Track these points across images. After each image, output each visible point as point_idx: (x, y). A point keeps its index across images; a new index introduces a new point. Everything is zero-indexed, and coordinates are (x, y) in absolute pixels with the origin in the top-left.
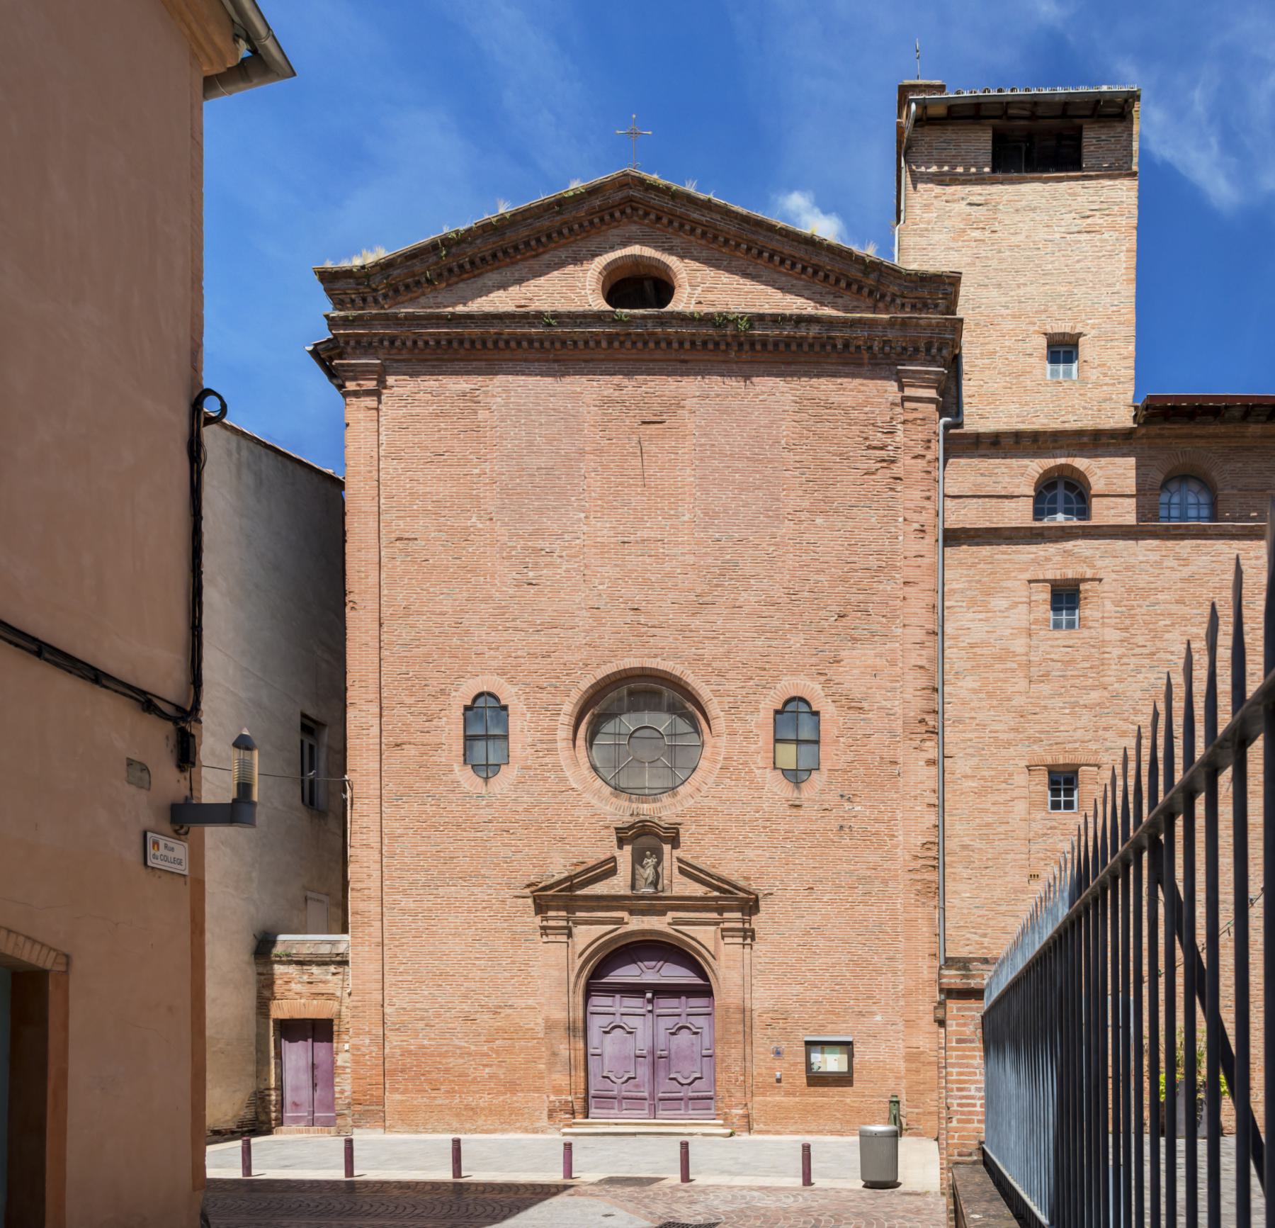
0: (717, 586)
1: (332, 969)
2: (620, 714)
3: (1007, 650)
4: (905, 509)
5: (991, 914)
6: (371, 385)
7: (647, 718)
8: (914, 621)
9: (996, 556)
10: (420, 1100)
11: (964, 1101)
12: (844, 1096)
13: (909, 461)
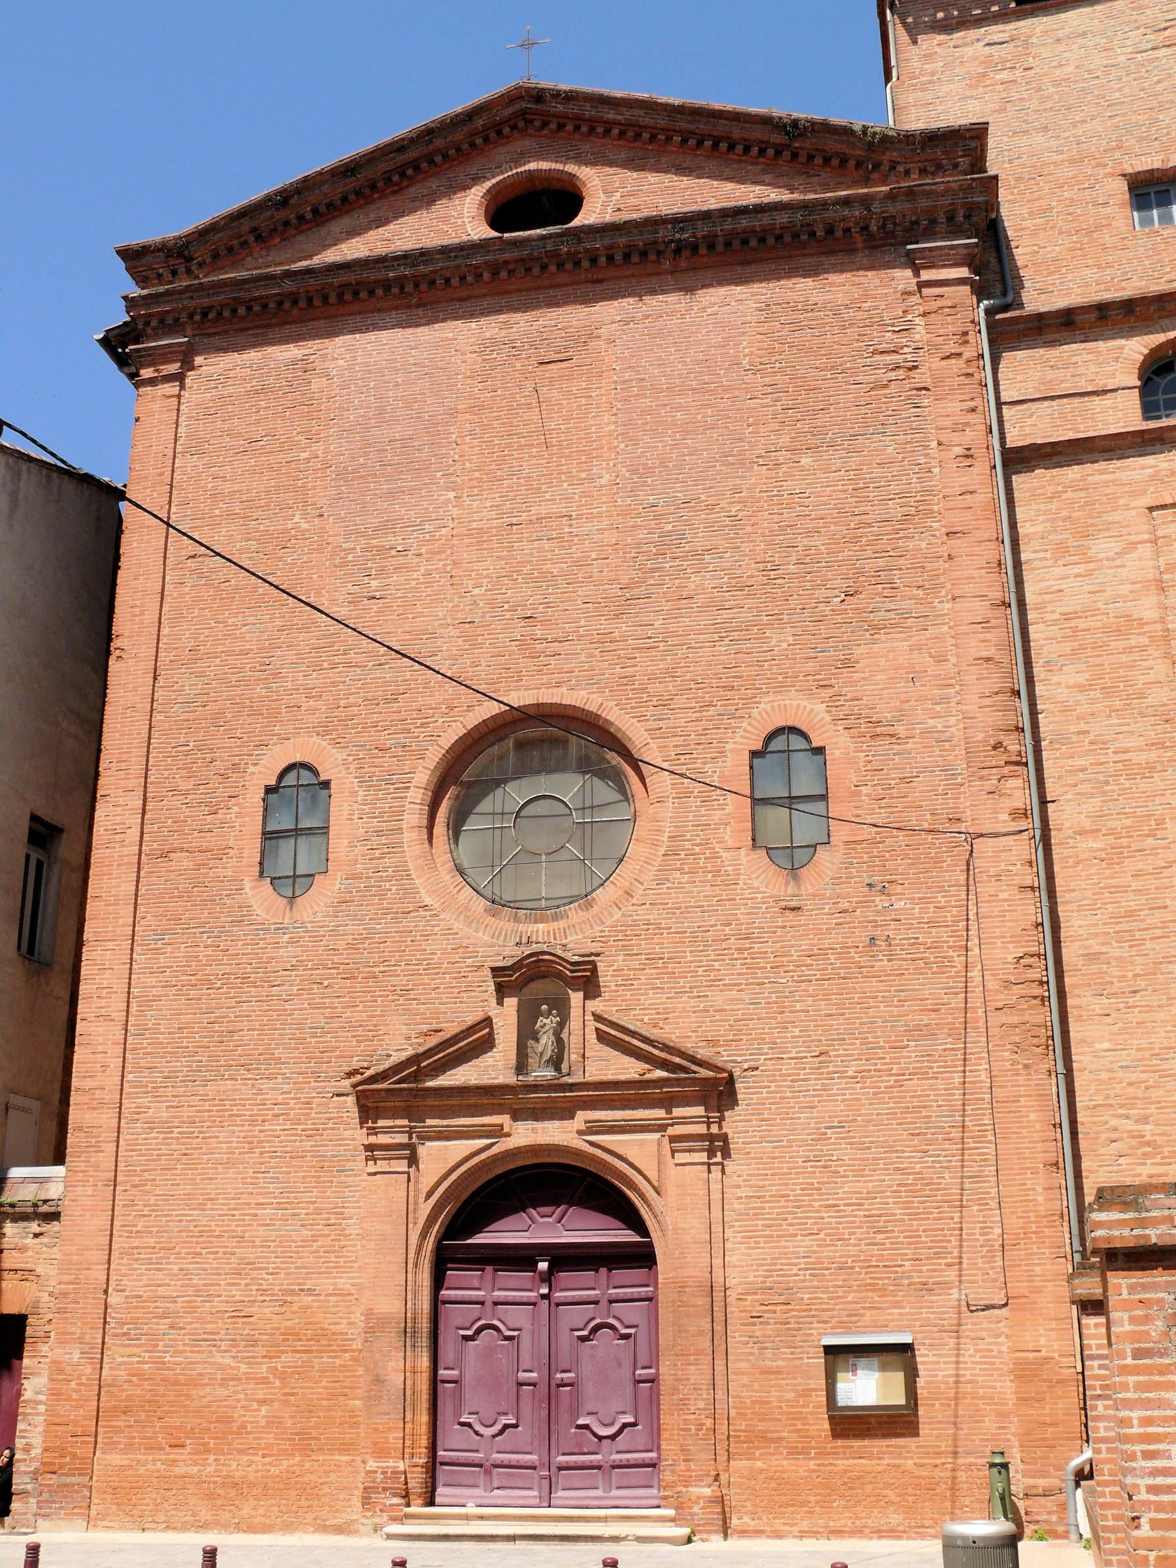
0: (653, 570)
1: (34, 1227)
2: (505, 781)
3: (1129, 618)
4: (937, 428)
5: (1152, 1079)
6: (173, 368)
7: (543, 784)
8: (968, 589)
9: (1090, 478)
10: (152, 1464)
11: (1160, 1480)
12: (900, 1456)
13: (936, 363)
